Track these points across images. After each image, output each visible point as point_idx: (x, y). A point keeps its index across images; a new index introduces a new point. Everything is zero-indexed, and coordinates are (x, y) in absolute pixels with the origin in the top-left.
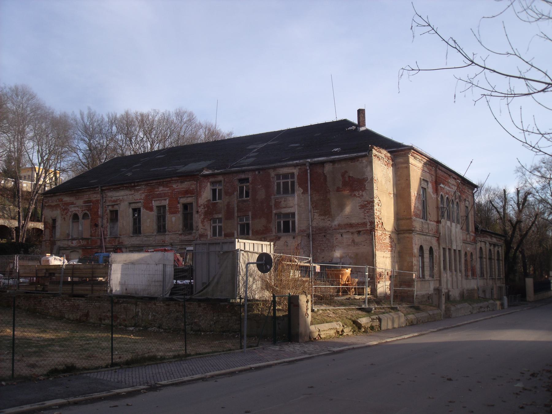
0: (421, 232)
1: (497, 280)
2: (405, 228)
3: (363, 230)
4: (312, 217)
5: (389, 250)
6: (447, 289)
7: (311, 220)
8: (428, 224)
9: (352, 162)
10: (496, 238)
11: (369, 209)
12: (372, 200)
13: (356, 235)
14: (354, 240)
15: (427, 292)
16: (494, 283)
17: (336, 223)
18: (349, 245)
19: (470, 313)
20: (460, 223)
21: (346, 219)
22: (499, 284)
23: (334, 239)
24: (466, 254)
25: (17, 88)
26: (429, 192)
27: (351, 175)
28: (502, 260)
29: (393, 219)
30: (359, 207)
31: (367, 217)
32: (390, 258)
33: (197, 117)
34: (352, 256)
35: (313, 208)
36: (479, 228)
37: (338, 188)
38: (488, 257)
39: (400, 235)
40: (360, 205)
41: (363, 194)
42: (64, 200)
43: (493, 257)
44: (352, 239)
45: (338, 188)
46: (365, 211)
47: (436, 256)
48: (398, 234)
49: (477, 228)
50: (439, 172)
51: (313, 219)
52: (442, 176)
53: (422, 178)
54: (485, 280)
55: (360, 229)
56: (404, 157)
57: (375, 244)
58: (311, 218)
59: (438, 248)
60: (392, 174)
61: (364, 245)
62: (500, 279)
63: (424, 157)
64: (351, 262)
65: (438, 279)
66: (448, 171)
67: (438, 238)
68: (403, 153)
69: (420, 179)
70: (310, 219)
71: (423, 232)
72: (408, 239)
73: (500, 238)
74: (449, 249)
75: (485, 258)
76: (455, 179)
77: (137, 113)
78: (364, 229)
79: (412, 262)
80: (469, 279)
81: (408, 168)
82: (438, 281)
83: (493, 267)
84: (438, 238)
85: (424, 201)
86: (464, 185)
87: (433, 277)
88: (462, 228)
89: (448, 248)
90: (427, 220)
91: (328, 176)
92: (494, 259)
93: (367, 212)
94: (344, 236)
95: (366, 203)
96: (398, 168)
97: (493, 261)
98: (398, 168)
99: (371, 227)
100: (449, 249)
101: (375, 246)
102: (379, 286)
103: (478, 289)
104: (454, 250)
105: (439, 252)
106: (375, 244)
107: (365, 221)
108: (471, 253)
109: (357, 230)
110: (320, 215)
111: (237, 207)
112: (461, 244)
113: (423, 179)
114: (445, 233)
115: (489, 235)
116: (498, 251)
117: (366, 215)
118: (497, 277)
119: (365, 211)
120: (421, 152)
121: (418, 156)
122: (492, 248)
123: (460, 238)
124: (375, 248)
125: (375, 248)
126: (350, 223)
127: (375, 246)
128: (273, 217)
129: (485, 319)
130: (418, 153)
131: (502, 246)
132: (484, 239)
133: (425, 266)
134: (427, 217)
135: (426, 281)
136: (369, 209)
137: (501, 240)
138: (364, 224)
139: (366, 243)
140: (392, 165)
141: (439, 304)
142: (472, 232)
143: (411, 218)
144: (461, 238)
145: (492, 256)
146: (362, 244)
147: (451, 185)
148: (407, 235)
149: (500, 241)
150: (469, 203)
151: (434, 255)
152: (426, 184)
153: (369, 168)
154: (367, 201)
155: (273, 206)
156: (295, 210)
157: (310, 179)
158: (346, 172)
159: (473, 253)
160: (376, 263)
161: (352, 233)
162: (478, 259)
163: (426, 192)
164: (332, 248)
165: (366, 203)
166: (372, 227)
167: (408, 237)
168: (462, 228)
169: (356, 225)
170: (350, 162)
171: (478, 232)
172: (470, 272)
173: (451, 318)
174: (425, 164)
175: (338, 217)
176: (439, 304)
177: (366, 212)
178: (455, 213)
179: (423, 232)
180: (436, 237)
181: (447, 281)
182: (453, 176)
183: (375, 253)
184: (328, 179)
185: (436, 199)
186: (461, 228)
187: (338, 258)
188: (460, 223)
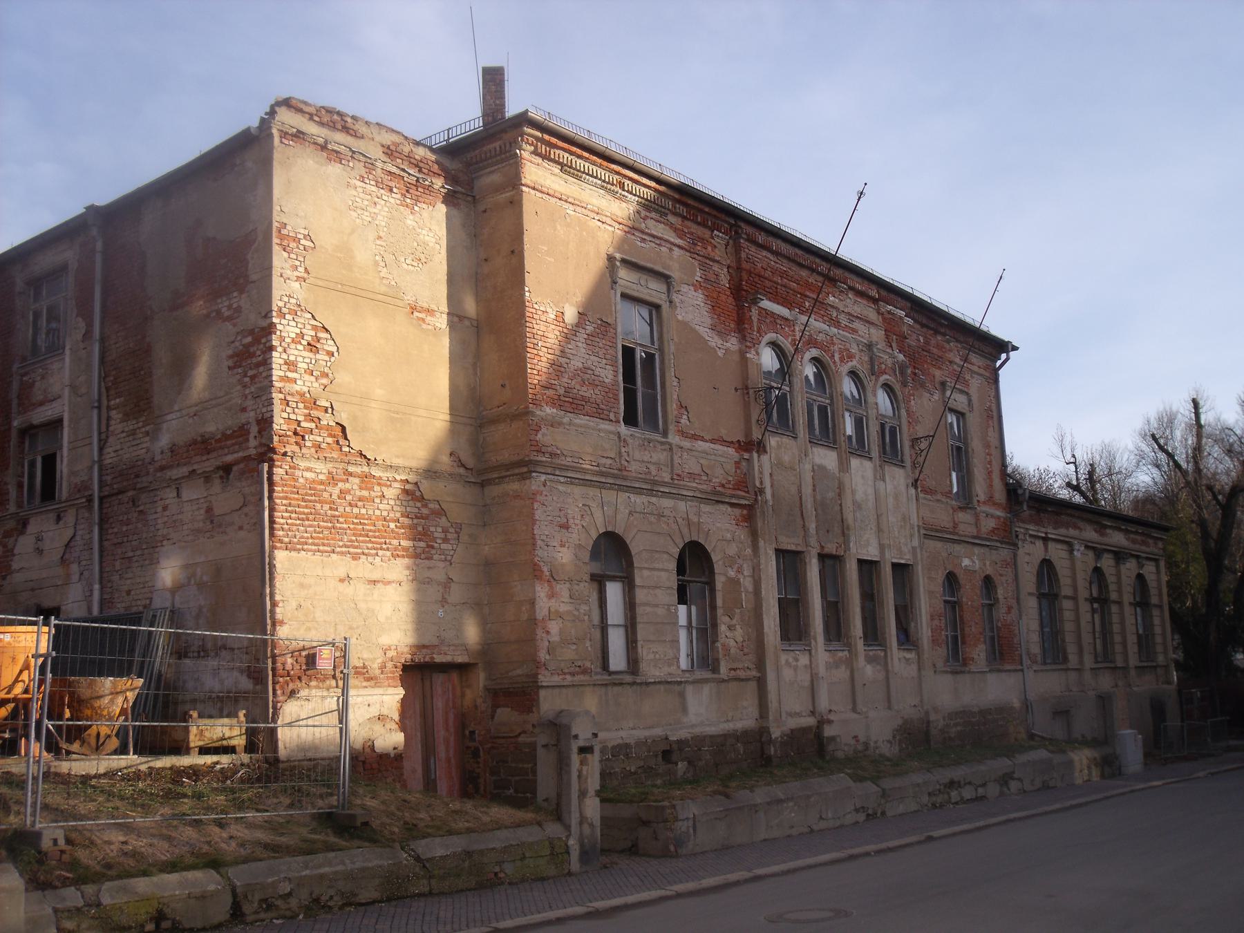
0: (615, 476)
1: (1133, 673)
2: (506, 456)
3: (237, 462)
4: (104, 429)
7: (100, 440)
8: (671, 449)
10: (1126, 532)
11: (258, 365)
12: (264, 323)
13: (217, 486)
14: (212, 509)
15: (658, 732)
16: (1120, 683)
17: (164, 441)
18: (199, 531)
19: (861, 817)
20: (908, 463)
21: (191, 421)
22: (1145, 685)
23: (160, 509)
24: (951, 580)
26: (685, 325)
28: (1160, 607)
29: (447, 417)
30: (230, 363)
31: (249, 403)
32: (406, 587)
33: (1042, 468)
34: (205, 578)
36: (1020, 492)
38: (1083, 593)
40: (230, 352)
43: (1114, 596)
44: (205, 505)
47: (734, 583)
49: (1015, 491)
50: (749, 250)
52: (783, 275)
53: (618, 256)
54: (1073, 676)
55: (229, 458)
59: (749, 551)
61: (241, 528)
62: (1155, 667)
63: (579, 151)
64: (203, 603)
67: (750, 508)
68: (497, 144)
69: (611, 259)
73: (1143, 534)
74: (831, 562)
75: (1156, 606)
79: (532, 603)
80: (969, 672)
81: (515, 204)
82: (753, 685)
83: (1116, 628)
84: (750, 508)
85: (959, 448)
86: (936, 332)
87: (715, 670)
88: (916, 481)
89: (814, 552)
90: (665, 434)
92: (1119, 603)
93: (253, 378)
94: (187, 494)
96: (485, 211)
97: (1114, 608)
98: (485, 211)
99: (261, 445)
100: (831, 562)
101: (272, 529)
102: (290, 709)
103: (1026, 705)
104: (868, 567)
105: (756, 570)
106: (271, 517)
107: (243, 418)
108: (988, 580)
109: (218, 463)
110: (127, 417)
112: (916, 543)
113: (624, 261)
114: (800, 492)
115: (1090, 522)
116: (1140, 577)
117: (247, 391)
118: (1133, 661)
119: (245, 376)
120: (587, 143)
122: (1107, 563)
123: (905, 519)
124: (272, 535)
125: (272, 535)
126: (202, 436)
127: (272, 529)
128: (12, 443)
129: (852, 858)
130: (574, 149)
131: (1156, 560)
132: (1063, 531)
133: (638, 620)
135: (647, 684)
136: (258, 365)
137: (1151, 541)
140: (449, 199)
142: (990, 500)
143: (523, 414)
144: (914, 520)
145: (1108, 592)
147: (844, 320)
149: (1144, 543)
150: (970, 401)
151: (720, 582)
152: (663, 288)
154: (251, 332)
155: (15, 402)
156: (61, 408)
159: (996, 579)
160: (274, 604)
161: (207, 478)
162: (1032, 604)
164: (150, 553)
165: (249, 339)
166: (264, 441)
167: (517, 497)
168: (916, 481)
169: (219, 441)
171: (1021, 504)
172: (982, 647)
173: (676, 856)
174: (648, 206)
176: (559, 796)
177: (247, 379)
179: (625, 478)
180: (732, 505)
181: (812, 681)
183: (272, 557)
185: (736, 357)
186: (910, 481)
188: (908, 463)
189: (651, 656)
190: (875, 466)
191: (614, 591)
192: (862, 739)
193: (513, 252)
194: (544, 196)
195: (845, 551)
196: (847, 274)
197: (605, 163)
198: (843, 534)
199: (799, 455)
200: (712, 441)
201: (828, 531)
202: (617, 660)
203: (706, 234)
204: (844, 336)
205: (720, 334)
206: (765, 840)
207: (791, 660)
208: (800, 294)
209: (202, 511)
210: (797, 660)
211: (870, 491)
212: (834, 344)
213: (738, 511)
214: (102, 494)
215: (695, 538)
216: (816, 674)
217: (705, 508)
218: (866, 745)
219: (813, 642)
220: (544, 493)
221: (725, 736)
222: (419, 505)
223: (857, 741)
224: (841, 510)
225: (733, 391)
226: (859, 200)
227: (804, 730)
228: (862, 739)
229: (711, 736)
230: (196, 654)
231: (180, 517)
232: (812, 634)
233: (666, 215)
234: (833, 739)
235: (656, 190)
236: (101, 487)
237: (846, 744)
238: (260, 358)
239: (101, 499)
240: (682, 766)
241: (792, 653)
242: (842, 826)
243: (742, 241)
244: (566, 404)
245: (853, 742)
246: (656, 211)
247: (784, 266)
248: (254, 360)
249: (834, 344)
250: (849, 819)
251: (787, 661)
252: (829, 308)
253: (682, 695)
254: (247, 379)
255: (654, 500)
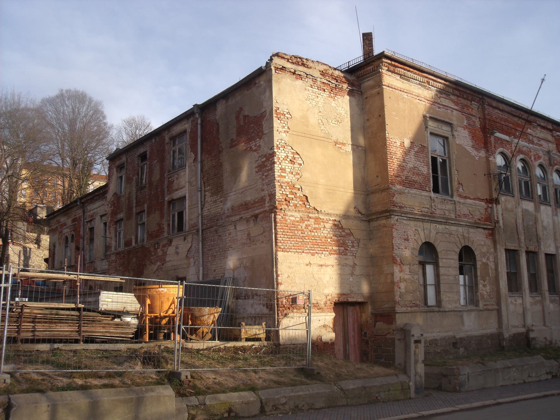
2: (379, 208)
4: (203, 200)
5: (334, 251)
6: (524, 326)
7: (201, 205)
8: (455, 203)
9: (248, 90)
11: (268, 170)
12: (271, 152)
13: (252, 224)
15: (451, 334)
17: (229, 205)
19: (550, 377)
21: (240, 196)
25: (43, 100)
26: (460, 146)
27: (246, 113)
29: (353, 191)
32: (336, 268)
34: (247, 264)
35: (204, 183)
37: (232, 140)
39: (371, 223)
41: (261, 144)
42: (61, 221)
44: (247, 232)
45: (232, 140)
46: (263, 175)
47: (486, 265)
48: (369, 221)
50: (489, 110)
51: (203, 203)
52: (506, 120)
53: (428, 115)
55: (257, 212)
56: (374, 75)
57: (276, 237)
58: (201, 202)
59: (492, 250)
60: (348, 108)
61: (262, 242)
63: (408, 68)
65: (496, 307)
66: (522, 113)
67: (493, 230)
68: (371, 67)
69: (424, 117)
70: (200, 203)
71: (434, 217)
72: (385, 229)
76: (551, 131)
77: (62, 90)
78: (262, 210)
79: (392, 274)
82: (495, 312)
84: (493, 230)
87: (477, 305)
90: (452, 196)
91: (220, 123)
93: (266, 176)
95: (264, 159)
98: (367, 98)
99: (271, 205)
100: (532, 255)
101: (276, 242)
102: (285, 322)
106: (276, 237)
107: (263, 194)
109: (252, 214)
111: (136, 198)
113: (430, 118)
114: (516, 222)
117: (264, 182)
119: (263, 175)
121: (409, 74)
124: (276, 245)
127: (276, 242)
130: (406, 67)
133: (441, 282)
134: (452, 191)
135: (446, 312)
138: (262, 200)
139: (265, 236)
141: (405, 362)
146: (259, 240)
147: (536, 141)
148: (383, 222)
151: (479, 264)
152: (449, 129)
153: (267, 94)
154: (265, 156)
156: (185, 192)
157: (201, 134)
158: (241, 109)
161: (248, 221)
163: (448, 143)
164: (224, 254)
167: (385, 226)
170: (246, 92)
175: (231, 194)
176: (405, 362)
177: (264, 177)
178: (550, 189)
179: (434, 217)
180: (484, 229)
181: (524, 311)
182: (538, 122)
183: (276, 255)
184: (221, 130)
185: (484, 160)
187: (231, 269)
189: (447, 299)
190: (553, 209)
191: (430, 269)
192: (549, 339)
193: (380, 116)
194: (393, 90)
195: (539, 250)
196: (536, 119)
197: (420, 73)
198: (538, 241)
199: (516, 205)
200: (474, 199)
201: (530, 240)
202: (431, 301)
203: (468, 103)
204: (536, 148)
205: (476, 149)
206: (502, 386)
207: (513, 301)
208: (514, 129)
209: (246, 235)
210: (516, 301)
211: (551, 221)
212: (531, 152)
213: (487, 232)
214: (203, 228)
215: (467, 244)
216: (526, 308)
217: (471, 230)
218: (551, 342)
219: (524, 293)
220: (397, 225)
221: (482, 336)
222: (341, 231)
223: (546, 340)
224: (536, 230)
225: (483, 176)
226: (542, 83)
227: (520, 334)
228: (549, 339)
229: (476, 336)
230: (243, 298)
231: (236, 237)
232: (523, 289)
233: (449, 95)
234: (534, 339)
235: (444, 84)
236: (202, 225)
237: (541, 341)
238: (269, 167)
239: (202, 230)
240: (462, 350)
241: (514, 298)
242: (540, 381)
243: (485, 106)
244: (406, 184)
245: (544, 340)
246: (445, 94)
247: (506, 116)
248: (267, 168)
249: (531, 152)
250: (544, 377)
251: (511, 301)
252: (528, 135)
253: (462, 317)
254: (264, 177)
255: (447, 227)
